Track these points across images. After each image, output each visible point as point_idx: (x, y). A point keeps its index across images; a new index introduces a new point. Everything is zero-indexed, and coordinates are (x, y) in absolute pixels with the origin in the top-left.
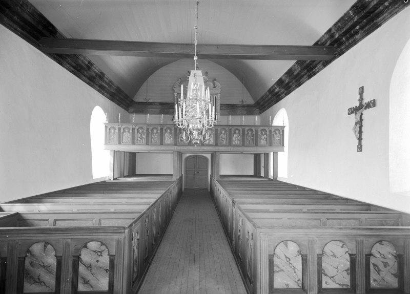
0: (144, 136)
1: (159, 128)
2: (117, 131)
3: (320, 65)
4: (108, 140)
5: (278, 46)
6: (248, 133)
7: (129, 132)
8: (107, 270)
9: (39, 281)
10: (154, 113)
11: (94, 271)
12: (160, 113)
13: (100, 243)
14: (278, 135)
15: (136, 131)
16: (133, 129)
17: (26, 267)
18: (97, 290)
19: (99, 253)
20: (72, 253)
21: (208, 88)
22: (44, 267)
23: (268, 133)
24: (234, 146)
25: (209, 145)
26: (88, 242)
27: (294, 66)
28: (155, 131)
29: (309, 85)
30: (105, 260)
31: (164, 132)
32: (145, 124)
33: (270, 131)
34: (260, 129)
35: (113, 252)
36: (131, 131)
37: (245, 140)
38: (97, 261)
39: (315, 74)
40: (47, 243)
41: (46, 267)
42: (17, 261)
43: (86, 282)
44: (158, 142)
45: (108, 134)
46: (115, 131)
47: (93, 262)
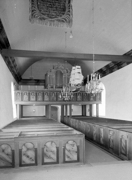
2: (20, 94)
3: (125, 64)
4: (16, 99)
5: (111, 55)
6: (85, 95)
7: (27, 95)
8: (76, 152)
9: (50, 157)
11: (71, 152)
13: (73, 141)
14: (99, 95)
16: (29, 93)
19: (73, 145)
22: (52, 151)
24: (32, 101)
25: (47, 101)
27: (110, 63)
28: (40, 94)
29: (117, 73)
30: (75, 148)
35: (79, 145)
37: (84, 98)
39: (121, 67)
40: (52, 142)
43: (69, 157)
44: (42, 99)
45: (16, 96)
46: (19, 95)
47: (71, 149)
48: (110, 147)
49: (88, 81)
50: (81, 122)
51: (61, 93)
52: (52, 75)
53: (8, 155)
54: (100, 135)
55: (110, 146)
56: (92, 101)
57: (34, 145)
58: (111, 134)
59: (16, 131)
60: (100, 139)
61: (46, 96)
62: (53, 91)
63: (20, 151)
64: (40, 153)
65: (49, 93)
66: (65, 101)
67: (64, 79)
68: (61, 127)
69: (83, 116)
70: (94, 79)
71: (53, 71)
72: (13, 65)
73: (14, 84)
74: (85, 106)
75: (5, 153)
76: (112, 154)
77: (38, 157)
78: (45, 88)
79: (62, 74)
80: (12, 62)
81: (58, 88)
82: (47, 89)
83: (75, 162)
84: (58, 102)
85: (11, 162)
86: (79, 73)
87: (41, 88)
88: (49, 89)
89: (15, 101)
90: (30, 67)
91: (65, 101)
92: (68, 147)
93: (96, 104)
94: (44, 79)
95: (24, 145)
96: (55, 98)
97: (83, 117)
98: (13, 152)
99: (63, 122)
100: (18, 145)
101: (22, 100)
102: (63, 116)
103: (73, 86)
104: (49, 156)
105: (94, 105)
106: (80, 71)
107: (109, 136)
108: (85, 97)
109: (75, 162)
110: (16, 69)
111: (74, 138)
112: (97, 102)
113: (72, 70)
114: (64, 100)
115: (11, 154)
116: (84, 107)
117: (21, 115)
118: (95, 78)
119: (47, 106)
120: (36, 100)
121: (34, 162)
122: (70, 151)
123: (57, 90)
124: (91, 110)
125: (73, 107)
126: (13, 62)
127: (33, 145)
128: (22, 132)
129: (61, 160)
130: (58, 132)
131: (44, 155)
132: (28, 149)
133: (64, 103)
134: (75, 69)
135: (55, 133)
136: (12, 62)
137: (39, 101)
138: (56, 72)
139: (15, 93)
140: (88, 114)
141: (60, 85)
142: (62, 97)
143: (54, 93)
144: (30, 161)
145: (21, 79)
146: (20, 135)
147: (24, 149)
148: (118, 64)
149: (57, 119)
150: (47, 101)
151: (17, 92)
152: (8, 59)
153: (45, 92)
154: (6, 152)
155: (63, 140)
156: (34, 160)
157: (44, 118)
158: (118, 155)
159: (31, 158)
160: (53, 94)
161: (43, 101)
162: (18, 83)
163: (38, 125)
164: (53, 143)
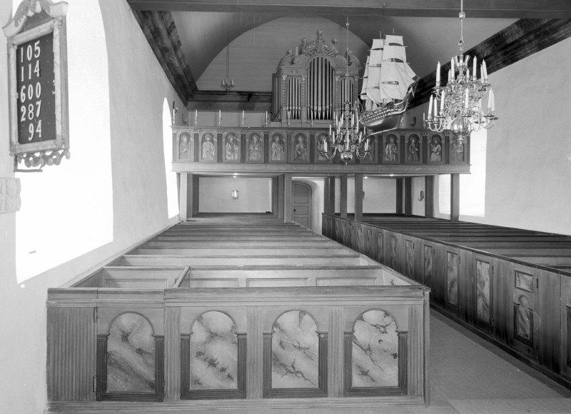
0: (237, 148)
1: (262, 134)
2: (192, 139)
4: (178, 156)
6: (410, 143)
7: (212, 141)
8: (395, 356)
9: (293, 371)
10: (225, 110)
11: (375, 356)
12: (240, 109)
15: (224, 140)
16: (220, 137)
17: (273, 350)
18: (381, 385)
20: (343, 328)
21: (484, 63)
22: (300, 348)
23: (443, 142)
24: (230, 162)
25: (277, 163)
26: (365, 312)
28: (255, 138)
30: (391, 340)
31: (270, 140)
32: (239, 128)
33: (425, 139)
34: (407, 135)
35: (405, 327)
36: (215, 140)
38: (380, 341)
40: (302, 313)
41: (304, 350)
42: (262, 339)
43: (364, 373)
45: (178, 144)
46: (188, 140)
48: (519, 338)
49: (438, 84)
50: (399, 235)
51: (327, 135)
52: (296, 74)
53: (140, 351)
54: (474, 288)
55: (520, 332)
56: (435, 164)
57: (234, 322)
58: (523, 286)
59: (177, 260)
60: (474, 303)
61: (274, 146)
62: (302, 129)
63: (185, 341)
64: (255, 351)
65: (284, 134)
66: (342, 163)
67: (336, 90)
68: (330, 252)
69: (399, 214)
70: (460, 78)
71: (302, 61)
72: (167, 43)
73: (173, 106)
74: (409, 180)
75: (132, 347)
76: (528, 363)
77: (248, 368)
78: (272, 120)
79: (329, 71)
80: (164, 33)
81: (322, 118)
82: (280, 121)
83: (388, 391)
84: (315, 168)
85: (153, 379)
86: (398, 60)
87: (256, 118)
88: (286, 120)
89: (174, 160)
90: (225, 50)
91: (342, 163)
92: (363, 334)
93: (450, 175)
94: (270, 89)
95: (199, 318)
96: (307, 154)
97: (402, 218)
98: (160, 342)
99: (330, 233)
100: (179, 317)
101: (196, 160)
102: (329, 214)
103: (375, 107)
104: (289, 364)
105: (442, 177)
106: (401, 53)
107: (515, 295)
108: (415, 144)
109: (388, 391)
110: (180, 56)
111: (387, 302)
112: (455, 169)
113: (372, 52)
114: (337, 161)
115: (152, 349)
116: (404, 187)
117: (194, 208)
118: (465, 73)
119: (278, 181)
120: (243, 160)
121: (234, 385)
122: (369, 349)
123: (314, 124)
124: (432, 194)
125: (369, 185)
126: (169, 33)
127: (231, 322)
128: (194, 269)
129: (335, 382)
130: (322, 273)
131: (271, 360)
132: (213, 336)
133: (339, 168)
134: (382, 49)
135: (310, 278)
136: (164, 33)
137: (252, 162)
138: (312, 65)
139: (174, 135)
140: (419, 209)
141: (324, 108)
142: (329, 148)
143: (300, 134)
144: (220, 383)
145: (195, 90)
146: (186, 279)
147: (199, 336)
148: (539, 29)
149: (309, 222)
150: (277, 163)
151: (180, 133)
152: (153, 21)
153: (272, 133)
154: (134, 339)
155: (343, 306)
156: (236, 379)
157: (268, 219)
158: (558, 372)
159: (223, 370)
160: (300, 139)
161: (266, 160)
162: (185, 104)
163: (247, 244)
164: (307, 317)
